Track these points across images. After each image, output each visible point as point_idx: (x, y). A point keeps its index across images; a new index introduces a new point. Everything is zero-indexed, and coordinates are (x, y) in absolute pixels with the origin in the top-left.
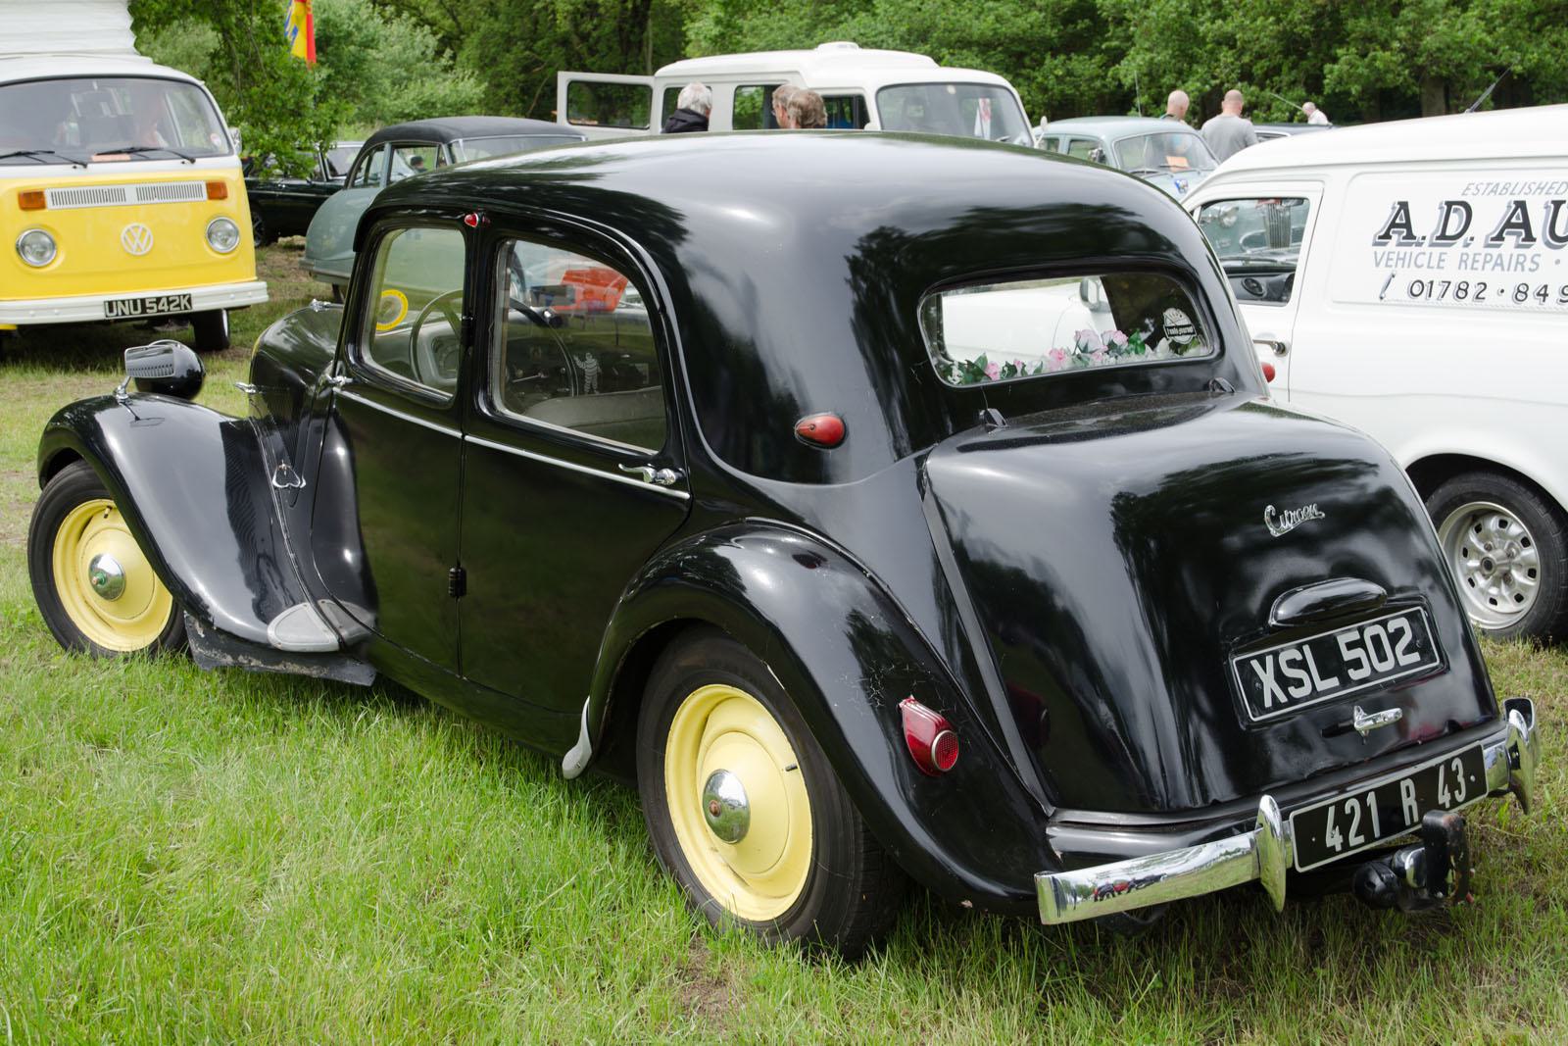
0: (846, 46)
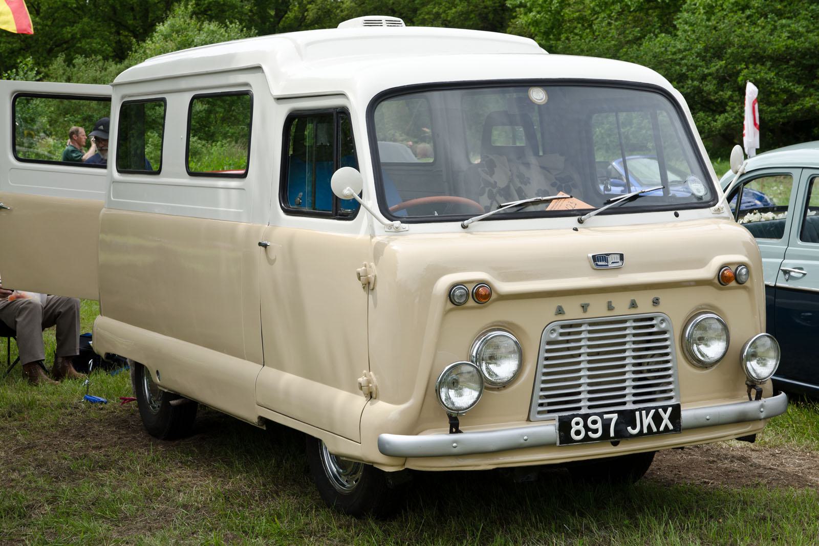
0: (379, 23)
